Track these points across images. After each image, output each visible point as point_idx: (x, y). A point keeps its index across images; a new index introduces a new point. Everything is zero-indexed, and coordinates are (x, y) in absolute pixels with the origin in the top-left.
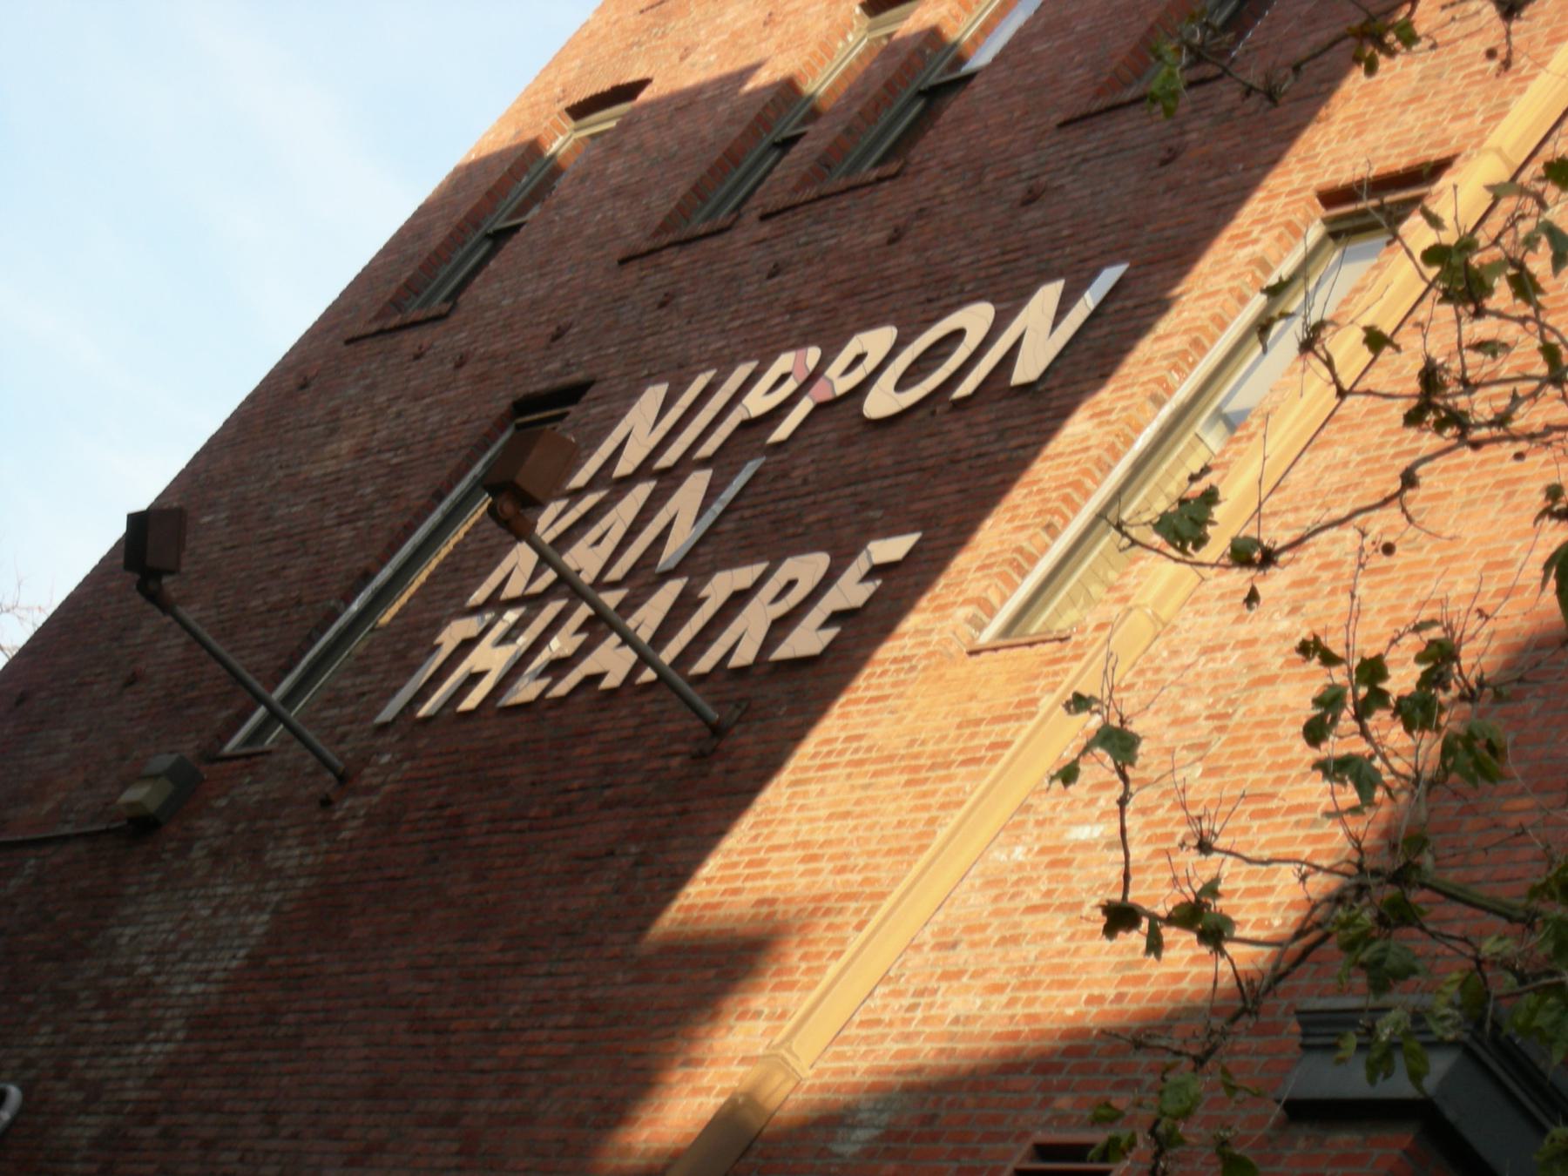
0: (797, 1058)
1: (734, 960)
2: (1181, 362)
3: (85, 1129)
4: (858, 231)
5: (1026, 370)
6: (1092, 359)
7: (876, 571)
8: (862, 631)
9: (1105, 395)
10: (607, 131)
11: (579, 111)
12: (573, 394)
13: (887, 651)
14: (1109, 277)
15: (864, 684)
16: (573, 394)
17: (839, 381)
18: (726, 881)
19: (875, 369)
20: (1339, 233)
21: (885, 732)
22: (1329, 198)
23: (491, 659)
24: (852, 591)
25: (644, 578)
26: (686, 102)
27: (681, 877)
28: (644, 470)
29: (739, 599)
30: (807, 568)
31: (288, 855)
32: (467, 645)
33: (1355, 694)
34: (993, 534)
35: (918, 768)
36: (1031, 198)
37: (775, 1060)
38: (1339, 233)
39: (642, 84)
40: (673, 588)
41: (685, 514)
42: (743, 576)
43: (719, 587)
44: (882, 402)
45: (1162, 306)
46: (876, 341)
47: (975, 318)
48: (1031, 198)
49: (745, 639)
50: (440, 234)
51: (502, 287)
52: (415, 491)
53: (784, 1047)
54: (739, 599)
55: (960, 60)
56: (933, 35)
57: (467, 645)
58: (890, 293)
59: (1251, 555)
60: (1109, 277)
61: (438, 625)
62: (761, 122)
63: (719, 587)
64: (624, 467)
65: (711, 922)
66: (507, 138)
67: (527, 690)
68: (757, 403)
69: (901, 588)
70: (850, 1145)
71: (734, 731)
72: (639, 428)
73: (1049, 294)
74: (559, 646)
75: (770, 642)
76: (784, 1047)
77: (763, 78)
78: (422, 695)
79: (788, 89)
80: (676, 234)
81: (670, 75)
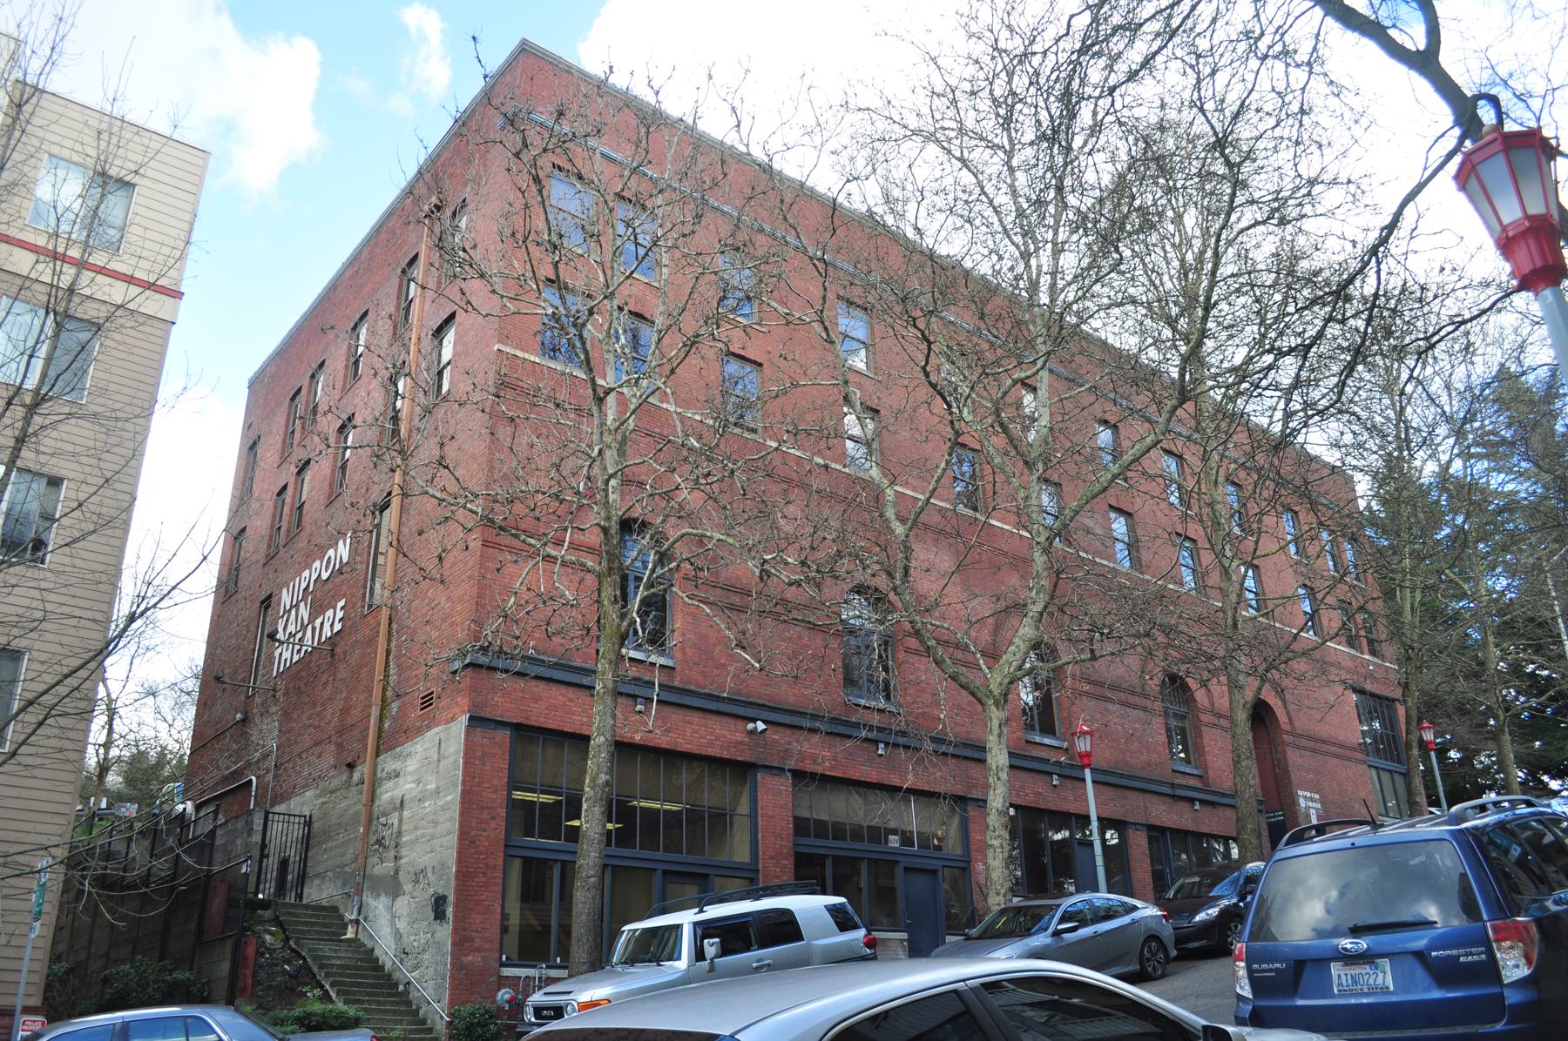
4: (301, 544)
10: (722, 900)
12: (270, 596)
16: (270, 596)
23: (286, 655)
25: (304, 628)
30: (330, 613)
31: (274, 709)
33: (1104, 841)
41: (304, 612)
43: (318, 622)
44: (325, 576)
46: (317, 564)
47: (331, 552)
49: (327, 632)
51: (245, 580)
52: (253, 628)
58: (849, 737)
63: (318, 622)
67: (296, 658)
68: (303, 586)
72: (286, 598)
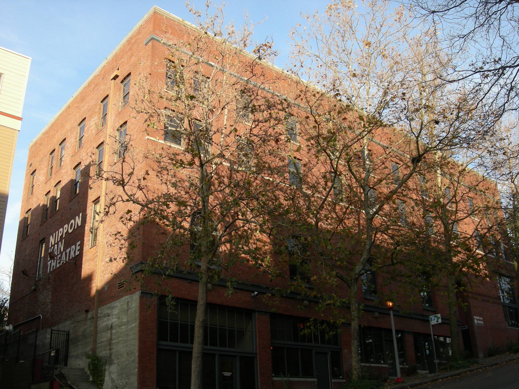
0: (94, 245)
1: (90, 278)
2: (90, 219)
3: (48, 315)
5: (80, 225)
6: (84, 221)
7: (79, 245)
8: (81, 250)
9: (86, 225)
11: (27, 213)
13: (84, 251)
14: (81, 214)
15: (84, 255)
17: (65, 231)
18: (85, 271)
19: (67, 228)
20: (95, 204)
21: (88, 258)
22: (93, 202)
24: (78, 248)
26: (36, 209)
27: (81, 275)
28: (55, 244)
29: (70, 252)
30: (74, 247)
32: (51, 264)
34: (86, 239)
35: (93, 260)
36: (70, 209)
37: (97, 286)
38: (95, 204)
39: (31, 209)
40: (64, 252)
42: (69, 249)
45: (86, 215)
46: (66, 226)
47: (73, 221)
48: (70, 209)
49: (72, 255)
50: (22, 229)
53: (98, 283)
54: (70, 252)
55: (76, 181)
56: (53, 196)
57: (51, 264)
59: (115, 259)
60: (81, 214)
61: (47, 263)
62: (43, 209)
64: (53, 244)
65: (86, 275)
66: (22, 218)
67: (58, 266)
68: (60, 235)
69: (82, 246)
70: (106, 289)
71: (77, 262)
73: (77, 217)
74: (58, 261)
75: (75, 254)
76: (98, 283)
77: (41, 205)
78: (50, 269)
79: (44, 205)
80: (43, 223)
81: (33, 207)
